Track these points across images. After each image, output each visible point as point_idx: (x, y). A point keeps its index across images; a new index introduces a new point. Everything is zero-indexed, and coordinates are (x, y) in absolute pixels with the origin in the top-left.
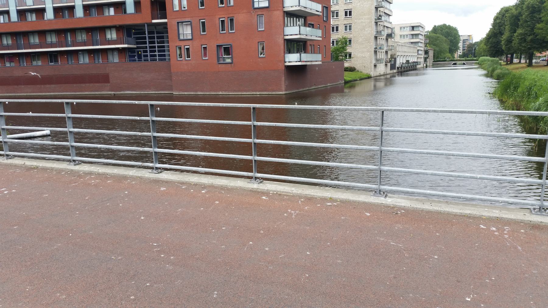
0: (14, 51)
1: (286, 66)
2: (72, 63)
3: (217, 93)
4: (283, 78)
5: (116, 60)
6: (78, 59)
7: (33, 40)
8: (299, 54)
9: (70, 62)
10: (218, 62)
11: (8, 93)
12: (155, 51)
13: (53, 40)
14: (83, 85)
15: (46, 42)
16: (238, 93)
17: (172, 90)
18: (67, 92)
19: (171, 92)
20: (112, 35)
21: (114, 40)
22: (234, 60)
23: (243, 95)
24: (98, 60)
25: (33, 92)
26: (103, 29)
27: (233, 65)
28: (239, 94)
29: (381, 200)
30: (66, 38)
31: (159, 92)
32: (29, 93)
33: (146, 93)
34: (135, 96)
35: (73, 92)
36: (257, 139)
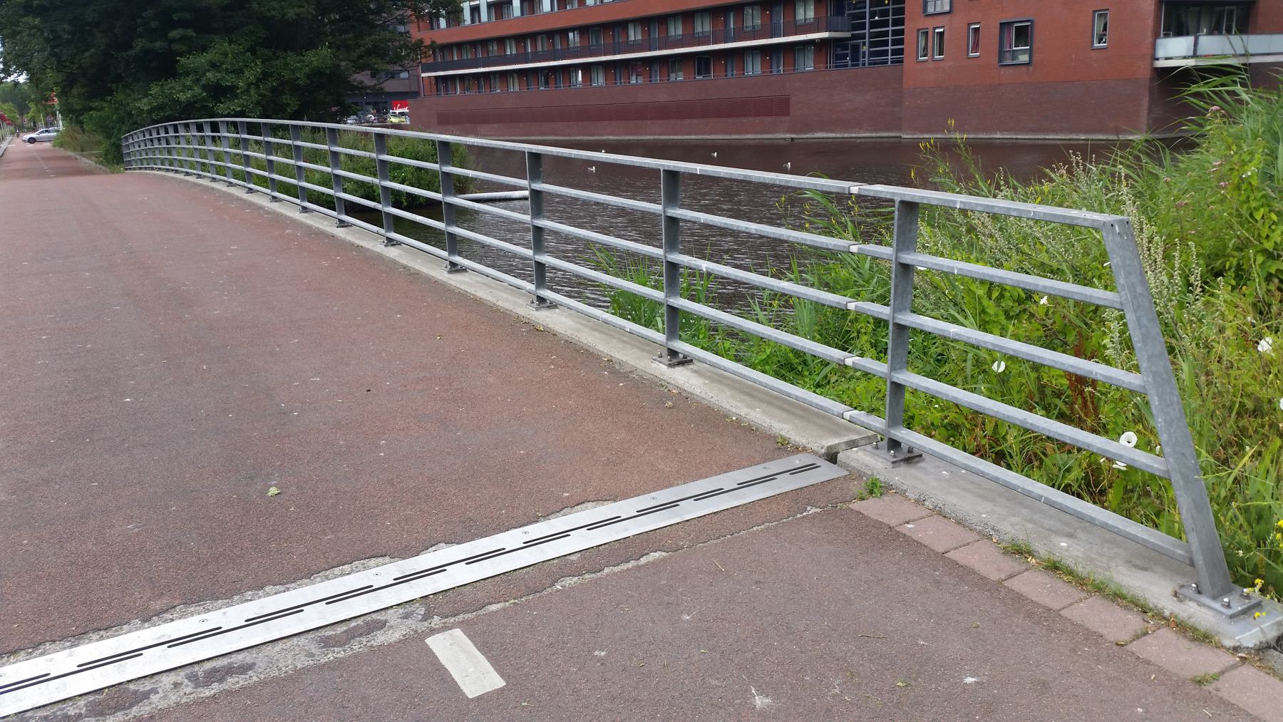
0: (794, 40)
1: (1158, 68)
3: (991, 136)
4: (1145, 101)
6: (795, 61)
8: (1191, 39)
9: (729, 73)
10: (1000, 61)
11: (627, 134)
12: (885, 43)
14: (744, 120)
15: (743, 28)
16: (1037, 137)
17: (899, 129)
18: (717, 133)
19: (898, 135)
21: (811, 24)
22: (1036, 57)
23: (1047, 141)
24: (778, 68)
25: (665, 134)
27: (1031, 68)
28: (1038, 139)
30: (726, 23)
31: (878, 135)
32: (658, 135)
33: (854, 135)
35: (726, 133)
36: (392, 207)
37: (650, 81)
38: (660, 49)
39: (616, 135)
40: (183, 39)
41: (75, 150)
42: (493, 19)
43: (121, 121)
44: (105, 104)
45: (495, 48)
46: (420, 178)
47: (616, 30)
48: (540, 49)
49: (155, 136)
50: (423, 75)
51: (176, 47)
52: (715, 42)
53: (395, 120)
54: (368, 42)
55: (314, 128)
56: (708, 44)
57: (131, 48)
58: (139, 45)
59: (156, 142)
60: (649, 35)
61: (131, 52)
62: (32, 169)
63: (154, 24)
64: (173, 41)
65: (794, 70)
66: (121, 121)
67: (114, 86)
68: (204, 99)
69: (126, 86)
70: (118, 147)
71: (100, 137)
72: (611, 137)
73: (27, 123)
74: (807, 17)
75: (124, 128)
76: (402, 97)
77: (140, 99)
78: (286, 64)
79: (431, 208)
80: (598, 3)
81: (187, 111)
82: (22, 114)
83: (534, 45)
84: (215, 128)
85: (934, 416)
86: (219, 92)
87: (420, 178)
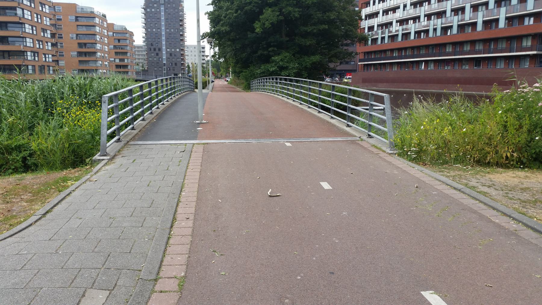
2: (490, 68)
5: (503, 66)
7: (526, 43)
13: (528, 44)
20: (527, 43)
21: (528, 47)
26: (520, 38)
29: (300, 106)
30: (490, 46)
34: (364, 87)
37: (454, 68)
38: (459, 55)
39: (436, 90)
40: (273, 50)
41: (235, 85)
42: (390, 42)
43: (251, 76)
44: (247, 71)
45: (389, 53)
46: (342, 99)
47: (441, 47)
48: (408, 54)
49: (261, 81)
50: (359, 63)
51: (271, 53)
52: (484, 54)
53: (346, 80)
54: (332, 52)
55: (310, 82)
56: (481, 54)
57: (257, 53)
58: (260, 52)
59: (261, 83)
60: (455, 50)
61: (257, 55)
62: (223, 89)
63: (265, 46)
64: (270, 51)
65: (519, 67)
66: (251, 76)
67: (251, 65)
68: (277, 71)
69: (253, 65)
70: (249, 84)
71: (244, 81)
72: (433, 91)
73: (219, 76)
74: (528, 44)
75: (252, 78)
76: (350, 72)
77: (257, 70)
78: (304, 60)
79: (345, 108)
80: (434, 36)
81: (272, 74)
82: (218, 72)
83: (406, 52)
84: (276, 79)
85: (379, 132)
86: (282, 68)
87: (342, 99)
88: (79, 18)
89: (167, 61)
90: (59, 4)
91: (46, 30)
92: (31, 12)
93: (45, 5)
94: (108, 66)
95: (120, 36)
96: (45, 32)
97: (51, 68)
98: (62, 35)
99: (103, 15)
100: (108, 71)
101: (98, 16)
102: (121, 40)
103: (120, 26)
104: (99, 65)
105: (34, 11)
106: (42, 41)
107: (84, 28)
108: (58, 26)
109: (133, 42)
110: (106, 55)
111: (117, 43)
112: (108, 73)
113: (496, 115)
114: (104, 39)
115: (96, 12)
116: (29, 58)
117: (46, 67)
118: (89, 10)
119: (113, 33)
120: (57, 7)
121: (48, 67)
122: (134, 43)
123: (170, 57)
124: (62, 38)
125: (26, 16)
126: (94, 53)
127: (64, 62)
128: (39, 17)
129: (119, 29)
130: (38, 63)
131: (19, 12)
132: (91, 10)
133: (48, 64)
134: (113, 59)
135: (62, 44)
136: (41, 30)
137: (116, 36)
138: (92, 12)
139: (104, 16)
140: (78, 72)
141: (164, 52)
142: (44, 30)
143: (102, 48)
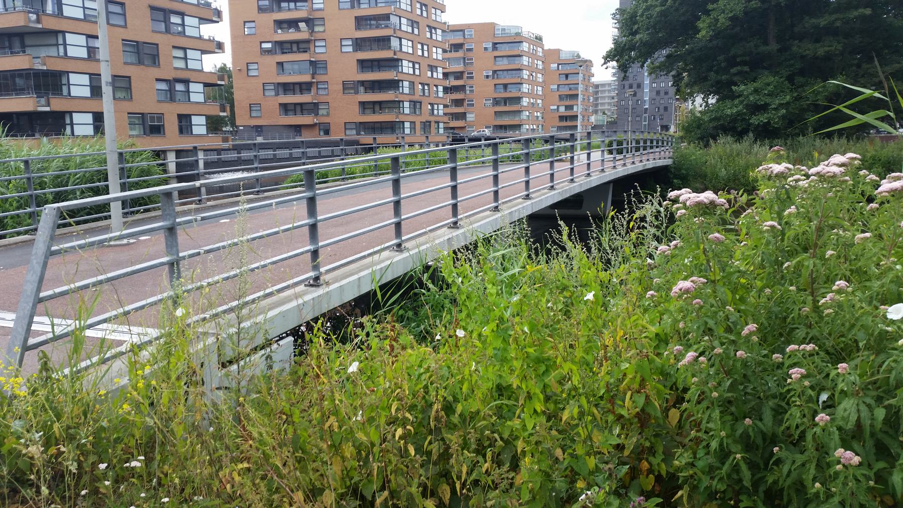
68: (745, 114)
88: (497, 46)
89: (650, 104)
90: (470, 26)
91: (436, 67)
92: (412, 41)
93: (435, 29)
94: (540, 118)
95: (568, 69)
96: (434, 70)
97: (441, 125)
98: (472, 73)
99: (536, 38)
100: (540, 127)
101: (527, 40)
102: (570, 76)
103: (570, 52)
104: (525, 118)
105: (417, 39)
106: (428, 85)
107: (505, 61)
108: (468, 59)
109: (589, 77)
110: (539, 101)
111: (563, 80)
112: (540, 130)
113: (842, 260)
114: (536, 75)
115: (525, 34)
116: (407, 111)
117: (433, 124)
118: (513, 31)
119: (559, 65)
120: (468, 32)
121: (436, 125)
122: (593, 80)
123: (658, 98)
124: (472, 78)
125: (404, 49)
126: (518, 100)
127: (473, 115)
128: (425, 48)
129: (568, 57)
130: (420, 117)
131: (394, 43)
132: (517, 31)
133: (437, 119)
134: (556, 107)
135: (472, 87)
136: (427, 68)
137: (562, 70)
138: (518, 34)
139: (539, 39)
140: (493, 130)
141: (647, 90)
142: (432, 68)
143: (533, 89)
